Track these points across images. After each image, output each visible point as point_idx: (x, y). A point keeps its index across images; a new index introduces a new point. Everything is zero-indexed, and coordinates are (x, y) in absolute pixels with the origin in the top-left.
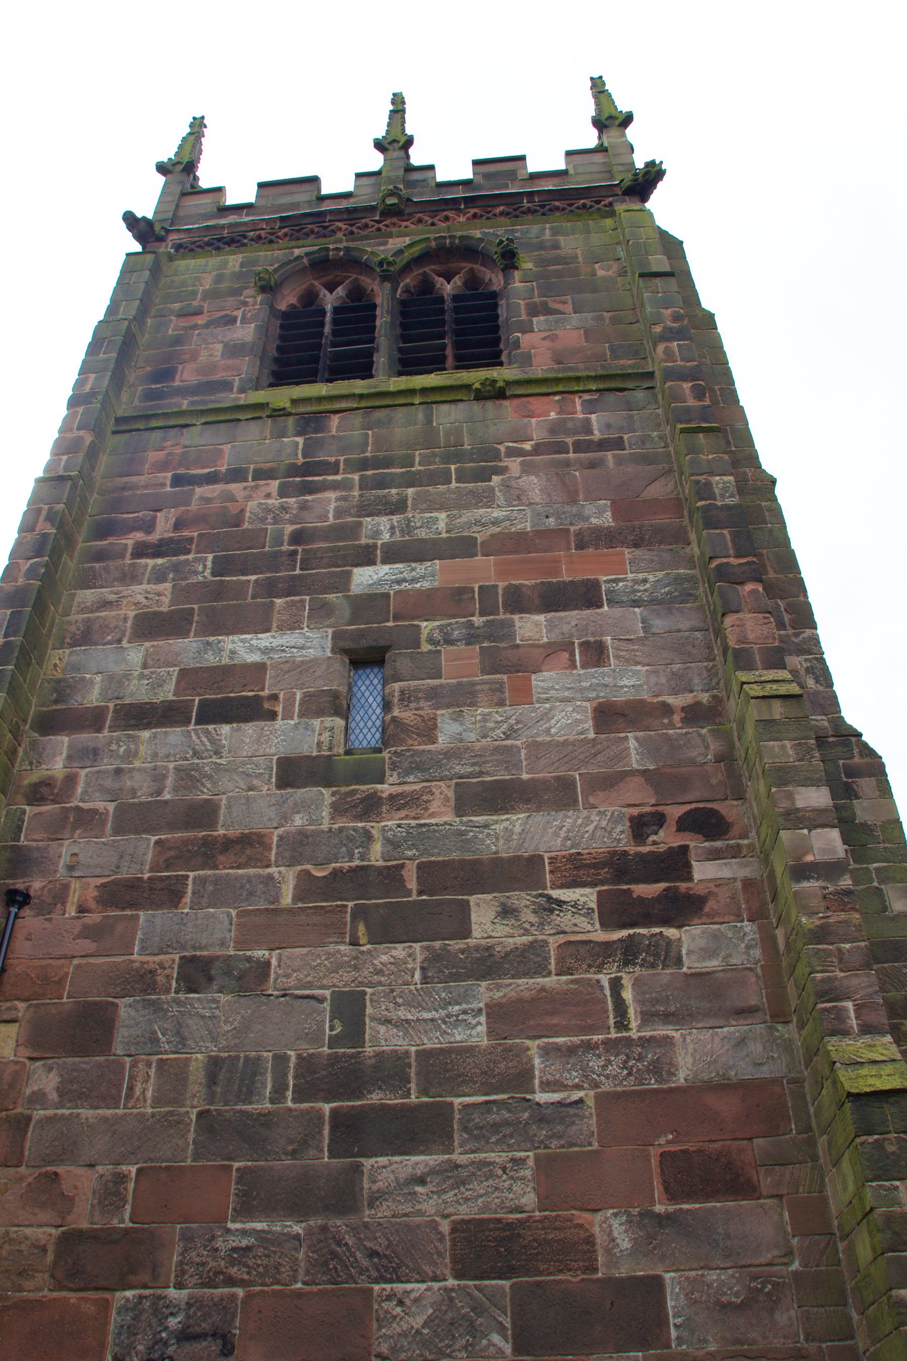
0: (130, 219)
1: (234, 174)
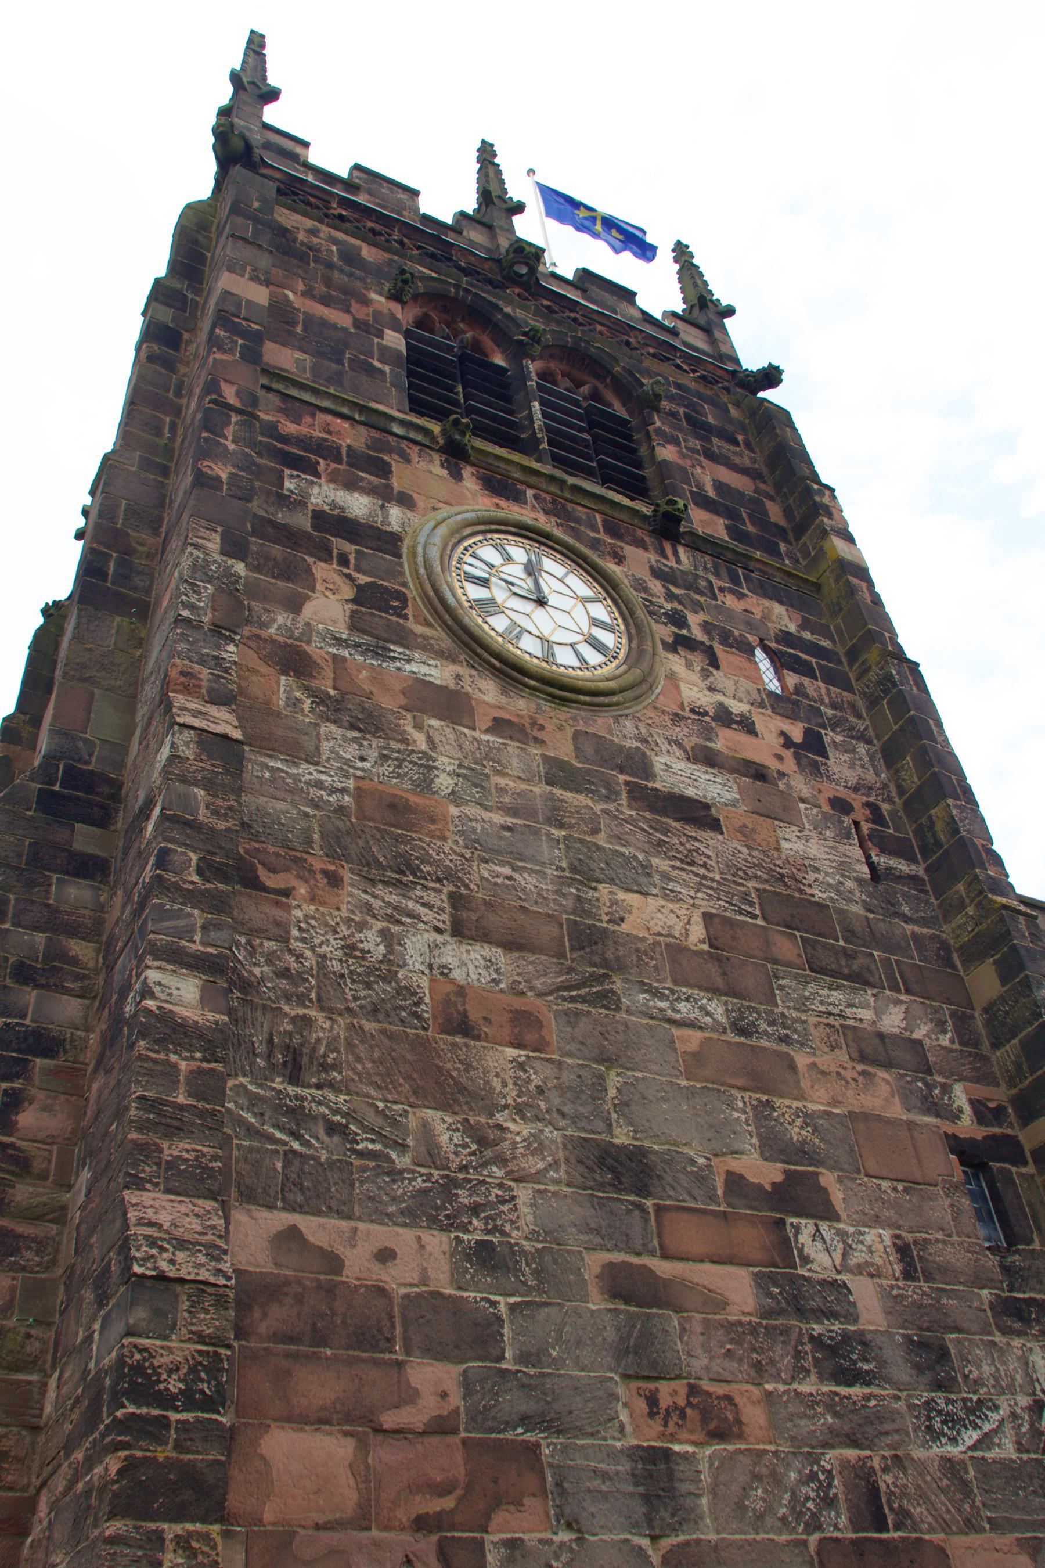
1: (332, 129)
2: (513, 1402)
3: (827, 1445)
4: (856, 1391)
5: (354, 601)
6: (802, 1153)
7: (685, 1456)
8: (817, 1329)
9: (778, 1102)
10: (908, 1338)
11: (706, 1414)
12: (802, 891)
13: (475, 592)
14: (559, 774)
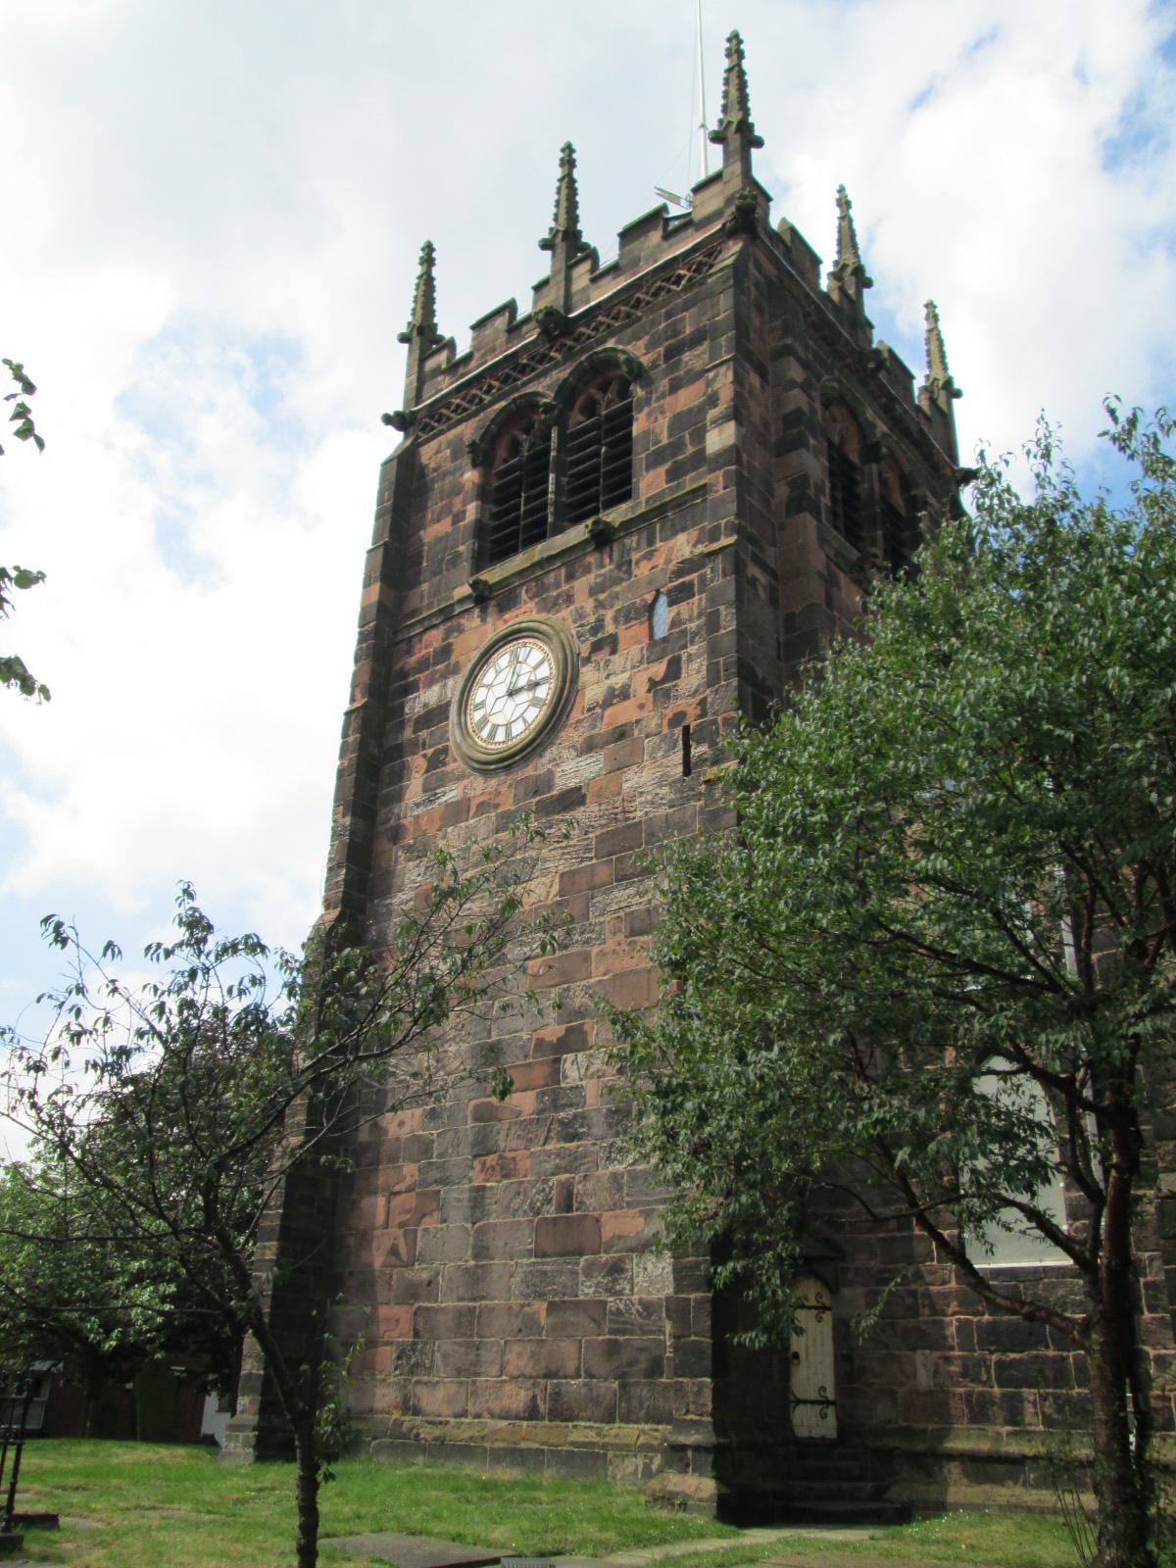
0: (388, 420)
2: (435, 1174)
3: (553, 1174)
4: (575, 1144)
5: (427, 771)
6: (581, 1013)
7: (492, 1188)
8: (562, 1115)
9: (573, 986)
10: (610, 1110)
11: (502, 1167)
12: (627, 819)
13: (500, 736)
14: (505, 821)
